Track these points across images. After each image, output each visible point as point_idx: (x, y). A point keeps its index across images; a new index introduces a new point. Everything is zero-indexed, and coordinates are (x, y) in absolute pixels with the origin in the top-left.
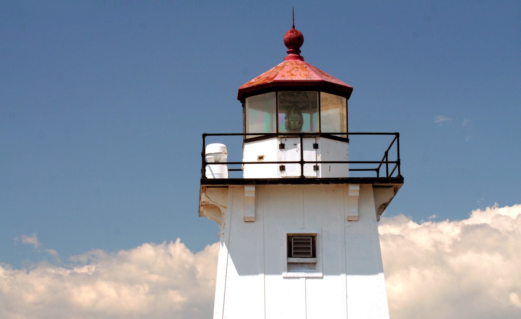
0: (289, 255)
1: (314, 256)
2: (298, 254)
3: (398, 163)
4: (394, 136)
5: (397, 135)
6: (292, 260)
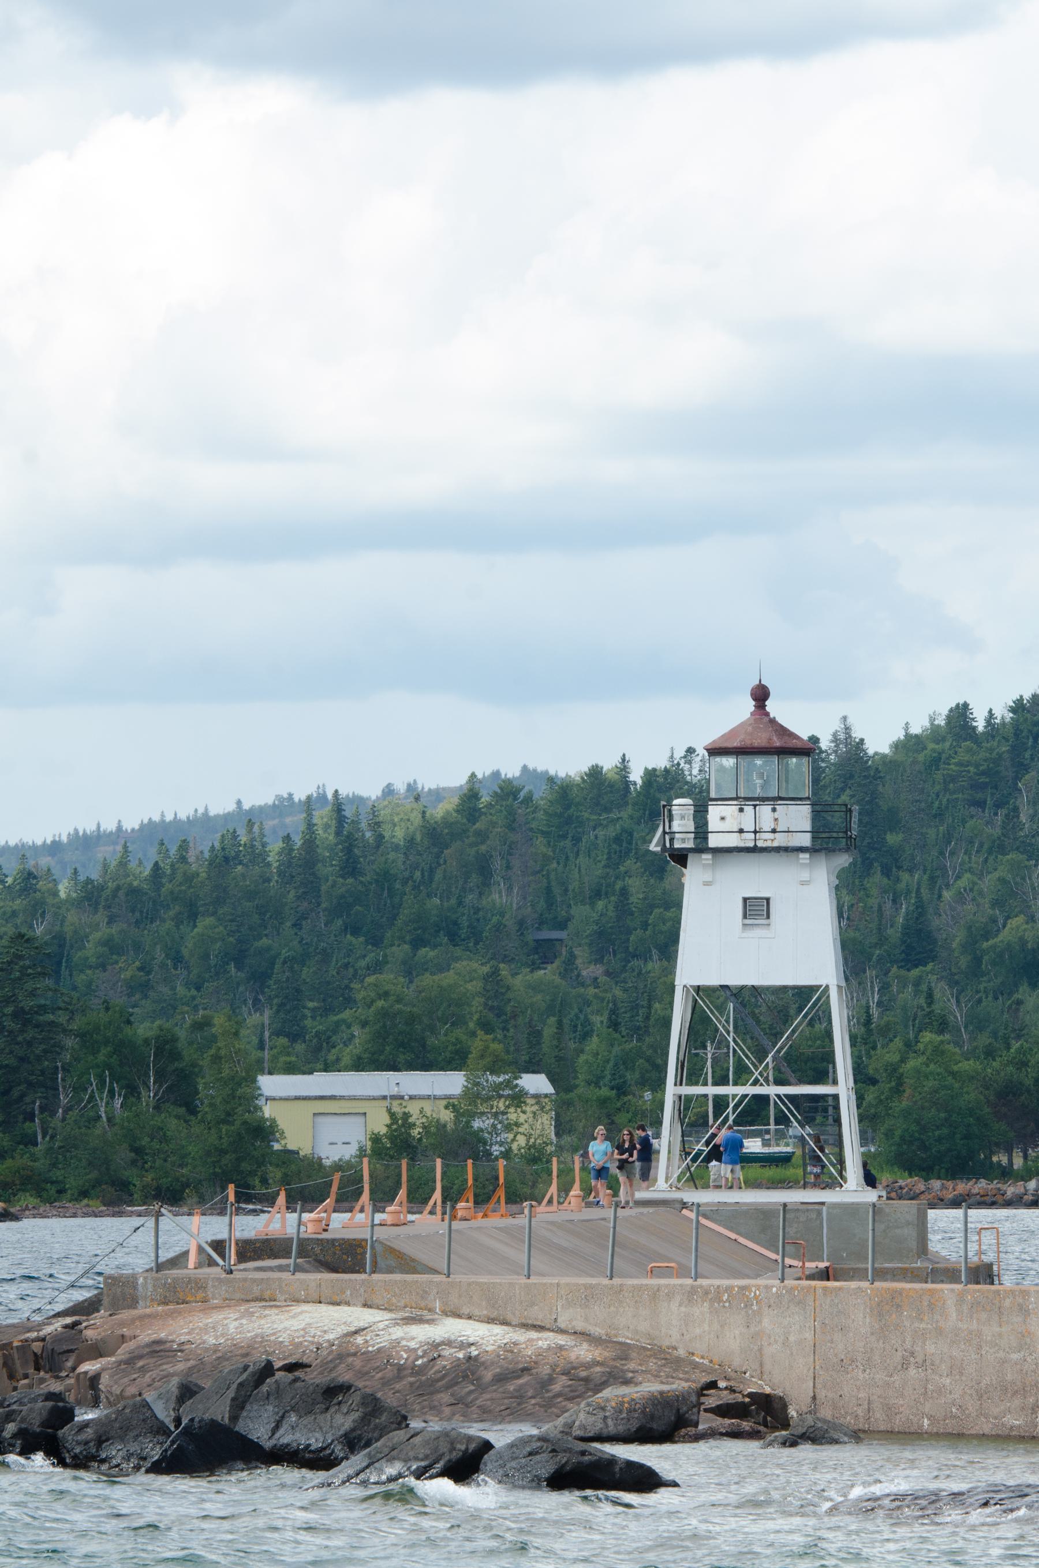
0: (745, 917)
1: (768, 917)
2: (754, 916)
6: (747, 921)
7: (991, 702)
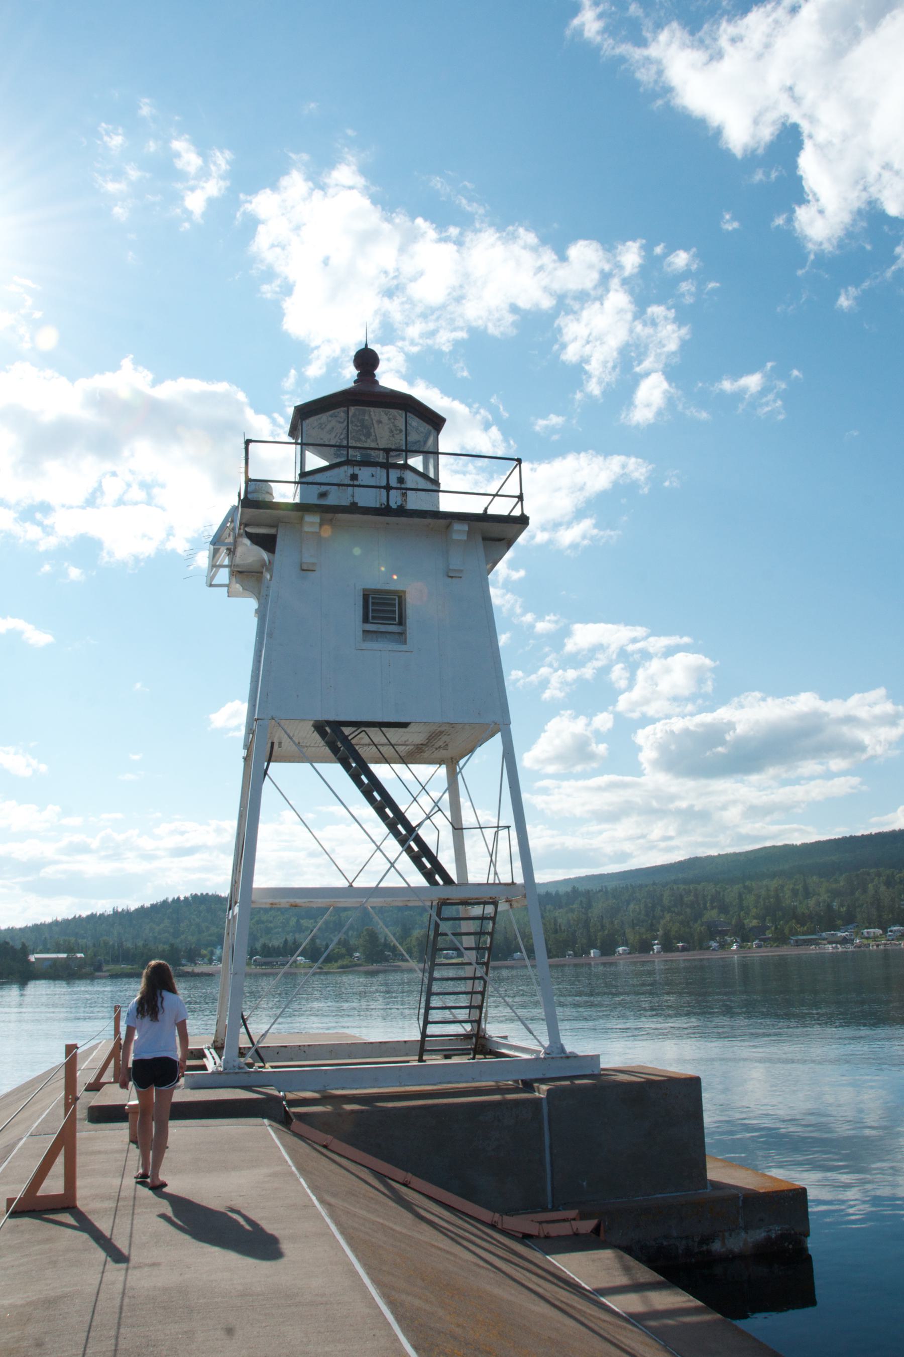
0: (366, 620)
1: (401, 622)
3: (520, 498)
4: (515, 463)
7: (147, 904)
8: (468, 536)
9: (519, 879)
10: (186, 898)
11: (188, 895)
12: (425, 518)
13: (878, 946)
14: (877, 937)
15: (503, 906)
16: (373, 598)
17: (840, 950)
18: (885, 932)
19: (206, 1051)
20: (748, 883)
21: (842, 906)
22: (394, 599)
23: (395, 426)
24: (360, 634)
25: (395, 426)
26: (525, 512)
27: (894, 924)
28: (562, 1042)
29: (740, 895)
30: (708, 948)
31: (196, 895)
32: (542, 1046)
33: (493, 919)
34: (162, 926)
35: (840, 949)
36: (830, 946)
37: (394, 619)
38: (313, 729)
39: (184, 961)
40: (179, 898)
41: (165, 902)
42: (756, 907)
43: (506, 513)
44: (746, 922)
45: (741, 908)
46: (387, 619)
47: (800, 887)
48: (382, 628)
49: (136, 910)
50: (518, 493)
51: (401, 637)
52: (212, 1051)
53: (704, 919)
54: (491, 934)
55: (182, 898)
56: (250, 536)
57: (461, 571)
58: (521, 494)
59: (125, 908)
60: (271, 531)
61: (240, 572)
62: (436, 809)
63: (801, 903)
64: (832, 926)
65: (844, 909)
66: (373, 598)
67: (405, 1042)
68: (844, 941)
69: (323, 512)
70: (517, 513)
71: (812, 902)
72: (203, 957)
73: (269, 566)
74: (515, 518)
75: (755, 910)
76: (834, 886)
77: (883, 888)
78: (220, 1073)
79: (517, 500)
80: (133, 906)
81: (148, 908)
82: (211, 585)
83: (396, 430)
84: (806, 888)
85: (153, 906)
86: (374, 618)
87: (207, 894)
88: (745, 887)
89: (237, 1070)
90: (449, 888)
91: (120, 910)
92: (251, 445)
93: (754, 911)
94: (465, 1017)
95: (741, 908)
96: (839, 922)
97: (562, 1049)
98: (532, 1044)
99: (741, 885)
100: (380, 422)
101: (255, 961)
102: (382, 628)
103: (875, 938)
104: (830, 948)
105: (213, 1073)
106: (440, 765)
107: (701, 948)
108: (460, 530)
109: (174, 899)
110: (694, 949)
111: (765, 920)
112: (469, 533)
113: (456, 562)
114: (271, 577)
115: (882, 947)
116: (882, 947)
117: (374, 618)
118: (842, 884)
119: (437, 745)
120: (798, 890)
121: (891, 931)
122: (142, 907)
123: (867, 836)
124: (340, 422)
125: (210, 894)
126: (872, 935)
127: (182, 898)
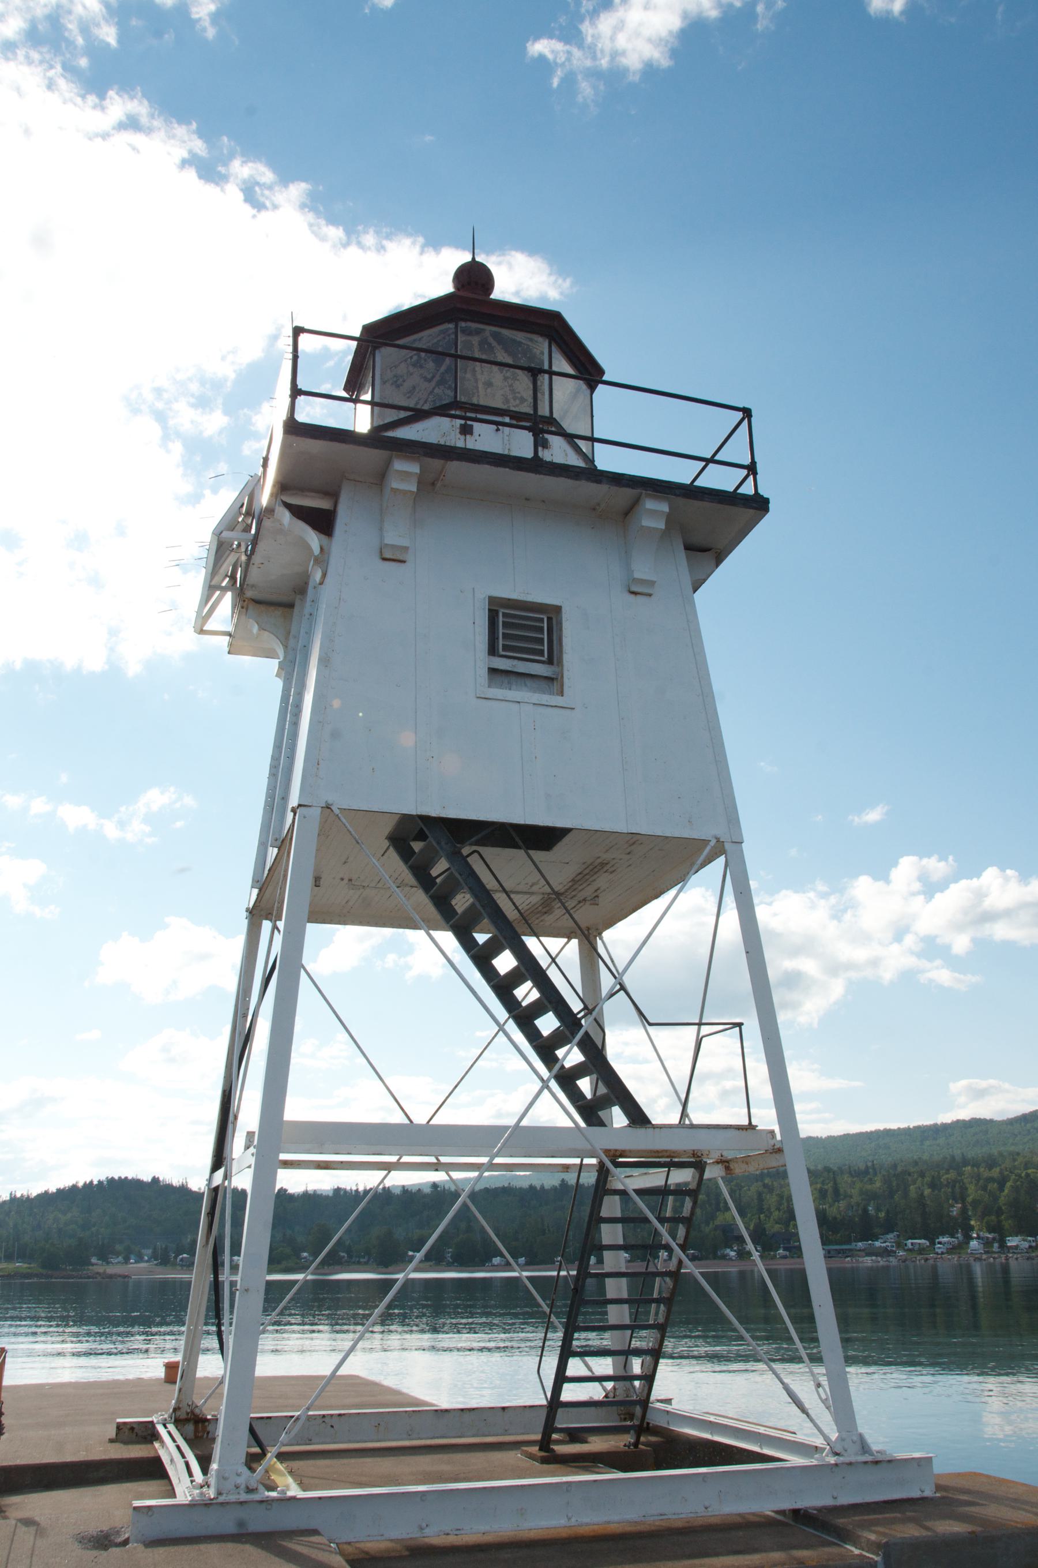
0: (492, 651)
1: (554, 658)
3: (752, 469)
4: (740, 415)
5: (747, 413)
8: (667, 523)
9: (766, 1118)
10: (100, 1182)
11: (103, 1178)
12: (599, 482)
13: (926, 1260)
14: (924, 1249)
15: (712, 1172)
16: (505, 615)
17: (882, 1263)
18: (933, 1243)
19: (160, 1428)
20: (767, 1181)
21: (880, 1211)
22: (542, 620)
23: (513, 391)
24: (484, 672)
25: (513, 391)
26: (761, 492)
27: (943, 1234)
28: (860, 1430)
29: (760, 1194)
30: (724, 1257)
31: (113, 1178)
32: (826, 1438)
33: (693, 1193)
34: (69, 1215)
35: (882, 1262)
36: (869, 1258)
37: (541, 653)
38: (387, 843)
39: (94, 1260)
40: (91, 1182)
41: (74, 1187)
42: (779, 1210)
43: (731, 488)
44: (767, 1226)
45: (761, 1210)
46: (532, 653)
47: (829, 1187)
48: (522, 667)
49: (39, 1196)
50: (747, 461)
51: (553, 682)
52: (171, 1427)
53: (717, 1222)
54: (688, 1221)
55: (95, 1182)
56: (288, 506)
57: (652, 583)
58: (753, 463)
59: (25, 1194)
60: (323, 504)
61: (257, 602)
62: (618, 987)
63: (830, 1207)
64: (868, 1234)
65: (882, 1215)
66: (505, 615)
67: (504, 1408)
68: (886, 1252)
69: (426, 455)
70: (748, 489)
71: (842, 1204)
72: (118, 1254)
73: (322, 559)
74: (745, 498)
75: (777, 1213)
76: (869, 1187)
77: (927, 1192)
78: (207, 1504)
79: (745, 472)
80: (35, 1190)
81: (53, 1194)
82: (202, 632)
83: (515, 399)
84: (836, 1191)
85: (59, 1191)
86: (506, 648)
87: (126, 1178)
88: (765, 1186)
89: (244, 1497)
90: (640, 1132)
91: (18, 1195)
92: (303, 338)
93: (776, 1214)
94: (609, 1371)
95: (761, 1210)
96: (877, 1230)
97: (864, 1447)
98: (807, 1435)
99: (760, 1183)
100: (489, 384)
101: (182, 1260)
102: (522, 667)
103: (921, 1251)
104: (868, 1261)
105: (192, 1506)
106: (569, 938)
107: (715, 1257)
108: (654, 513)
109: (85, 1183)
110: (707, 1258)
111: (788, 1226)
112: (670, 519)
113: (643, 569)
114: (324, 575)
115: (931, 1262)
116: (931, 1262)
117: (506, 648)
118: (878, 1184)
119: (581, 896)
120: (826, 1191)
121: (940, 1243)
122: (46, 1192)
123: (904, 1129)
124: (426, 380)
125: (130, 1177)
126: (917, 1247)
127: (95, 1182)
